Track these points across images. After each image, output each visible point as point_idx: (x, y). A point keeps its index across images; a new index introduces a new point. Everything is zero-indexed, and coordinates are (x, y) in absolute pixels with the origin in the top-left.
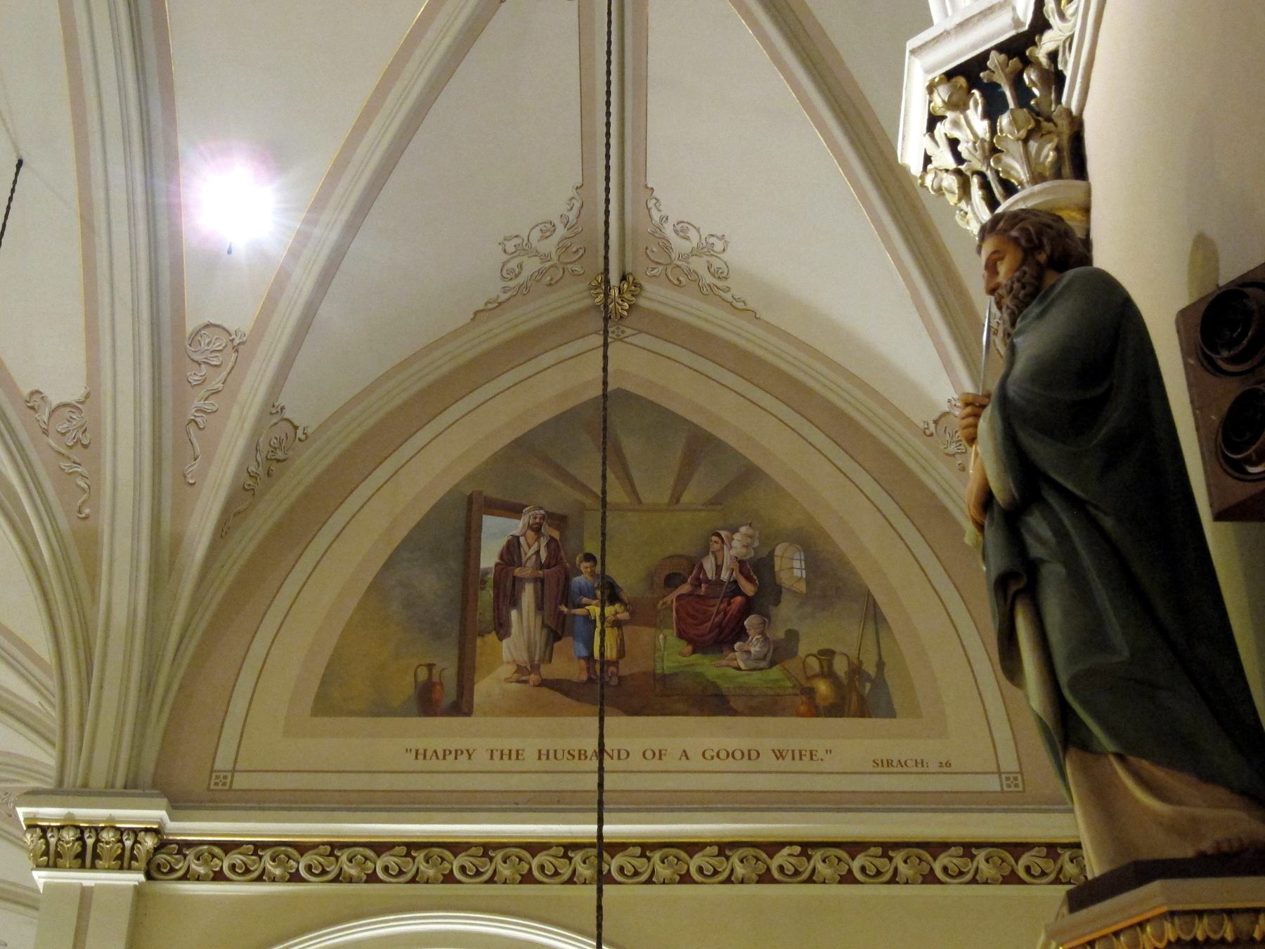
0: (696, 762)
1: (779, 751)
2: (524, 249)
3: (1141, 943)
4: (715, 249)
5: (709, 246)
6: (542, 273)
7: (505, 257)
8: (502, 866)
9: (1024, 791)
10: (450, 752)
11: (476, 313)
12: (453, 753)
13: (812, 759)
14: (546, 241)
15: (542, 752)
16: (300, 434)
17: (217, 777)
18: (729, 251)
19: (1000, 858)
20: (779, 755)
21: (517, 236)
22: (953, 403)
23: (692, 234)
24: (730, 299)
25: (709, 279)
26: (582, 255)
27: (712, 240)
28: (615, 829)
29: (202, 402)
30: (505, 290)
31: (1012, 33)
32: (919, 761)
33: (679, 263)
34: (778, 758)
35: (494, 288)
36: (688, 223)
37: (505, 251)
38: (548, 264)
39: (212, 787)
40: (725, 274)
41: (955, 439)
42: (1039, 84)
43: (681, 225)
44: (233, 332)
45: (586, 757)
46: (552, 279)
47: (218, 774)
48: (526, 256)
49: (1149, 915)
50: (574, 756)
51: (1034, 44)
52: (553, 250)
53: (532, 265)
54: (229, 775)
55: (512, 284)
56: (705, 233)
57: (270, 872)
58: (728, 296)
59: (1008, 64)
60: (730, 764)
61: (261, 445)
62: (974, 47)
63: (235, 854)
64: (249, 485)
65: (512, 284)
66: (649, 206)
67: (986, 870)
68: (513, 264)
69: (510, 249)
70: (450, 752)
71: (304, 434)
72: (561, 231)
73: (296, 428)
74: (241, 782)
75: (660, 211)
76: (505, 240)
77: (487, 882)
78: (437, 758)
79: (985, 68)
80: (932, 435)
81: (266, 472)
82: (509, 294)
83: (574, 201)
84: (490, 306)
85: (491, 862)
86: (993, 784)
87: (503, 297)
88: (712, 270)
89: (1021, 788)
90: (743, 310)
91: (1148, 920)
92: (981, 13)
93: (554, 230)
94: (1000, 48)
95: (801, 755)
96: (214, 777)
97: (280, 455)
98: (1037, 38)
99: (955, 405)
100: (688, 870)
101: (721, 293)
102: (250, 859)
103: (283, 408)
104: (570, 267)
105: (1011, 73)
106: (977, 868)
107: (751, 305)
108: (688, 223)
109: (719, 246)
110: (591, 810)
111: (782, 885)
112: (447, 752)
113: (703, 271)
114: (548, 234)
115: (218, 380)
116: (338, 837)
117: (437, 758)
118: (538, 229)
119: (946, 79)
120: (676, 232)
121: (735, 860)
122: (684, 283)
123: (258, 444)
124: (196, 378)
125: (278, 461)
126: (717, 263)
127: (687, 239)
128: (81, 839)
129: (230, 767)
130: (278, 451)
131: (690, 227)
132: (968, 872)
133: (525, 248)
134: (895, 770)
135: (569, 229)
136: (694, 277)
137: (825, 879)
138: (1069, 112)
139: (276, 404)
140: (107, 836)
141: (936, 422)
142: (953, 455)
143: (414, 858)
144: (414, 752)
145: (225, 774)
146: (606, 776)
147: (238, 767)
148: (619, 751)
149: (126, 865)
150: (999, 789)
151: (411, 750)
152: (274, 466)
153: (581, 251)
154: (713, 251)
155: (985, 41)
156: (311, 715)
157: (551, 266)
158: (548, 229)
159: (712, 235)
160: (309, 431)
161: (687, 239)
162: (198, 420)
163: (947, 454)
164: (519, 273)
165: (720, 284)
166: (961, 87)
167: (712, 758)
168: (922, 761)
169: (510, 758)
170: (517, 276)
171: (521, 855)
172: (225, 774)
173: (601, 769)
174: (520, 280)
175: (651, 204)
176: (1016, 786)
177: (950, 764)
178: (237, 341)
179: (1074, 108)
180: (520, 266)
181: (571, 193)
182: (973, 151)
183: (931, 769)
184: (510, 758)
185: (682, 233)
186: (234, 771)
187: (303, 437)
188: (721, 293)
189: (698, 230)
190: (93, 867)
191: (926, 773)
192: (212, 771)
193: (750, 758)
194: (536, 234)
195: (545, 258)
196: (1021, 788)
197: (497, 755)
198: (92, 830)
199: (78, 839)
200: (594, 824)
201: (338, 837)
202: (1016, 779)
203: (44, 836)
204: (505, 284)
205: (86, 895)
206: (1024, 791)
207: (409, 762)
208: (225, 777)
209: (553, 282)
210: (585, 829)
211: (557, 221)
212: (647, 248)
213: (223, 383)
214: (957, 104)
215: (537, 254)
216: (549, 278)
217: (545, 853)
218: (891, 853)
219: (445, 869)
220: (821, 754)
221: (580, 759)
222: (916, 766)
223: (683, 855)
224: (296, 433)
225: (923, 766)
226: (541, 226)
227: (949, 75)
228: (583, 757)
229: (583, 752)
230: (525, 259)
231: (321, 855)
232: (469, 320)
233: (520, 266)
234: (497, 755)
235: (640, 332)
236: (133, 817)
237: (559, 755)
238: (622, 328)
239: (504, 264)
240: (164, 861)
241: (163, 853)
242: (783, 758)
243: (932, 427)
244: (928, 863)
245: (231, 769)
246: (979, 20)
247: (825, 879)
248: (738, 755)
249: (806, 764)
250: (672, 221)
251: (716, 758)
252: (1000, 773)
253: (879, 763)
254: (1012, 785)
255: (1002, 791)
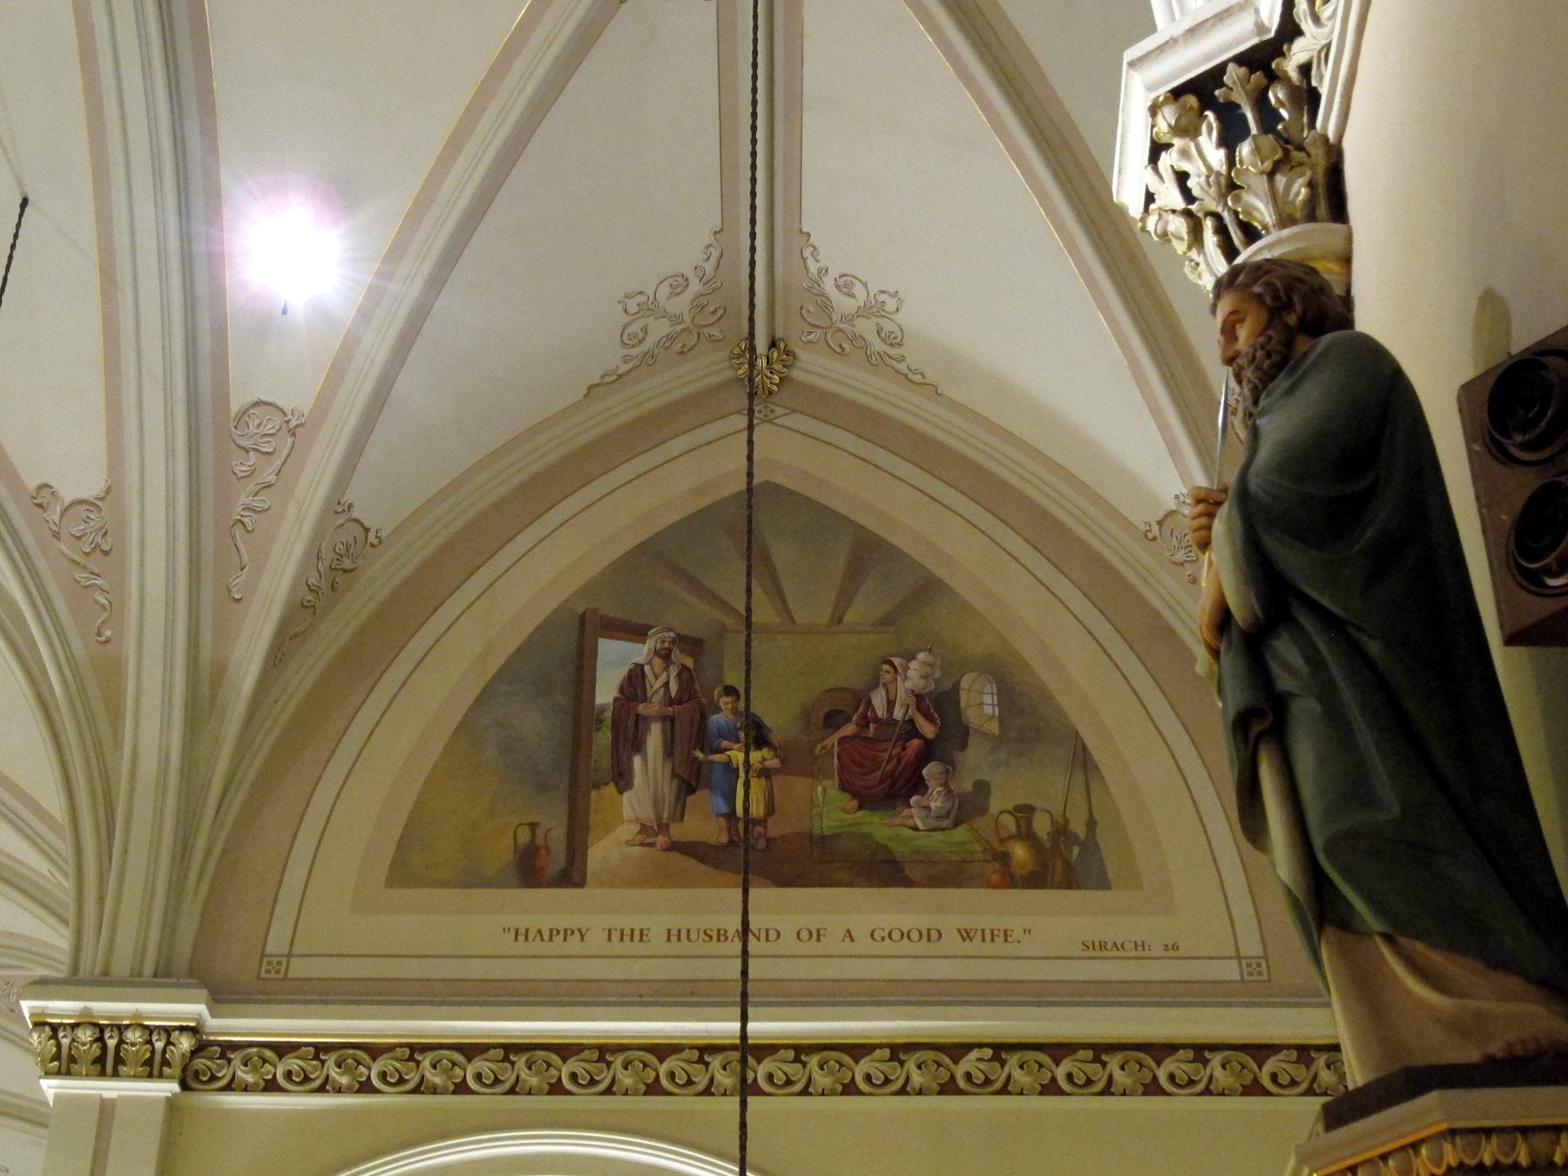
0: (863, 944)
1: (966, 930)
2: (650, 309)
3: (1415, 1169)
4: (886, 308)
5: (879, 305)
6: (672, 338)
7: (626, 319)
8: (622, 1073)
9: (1269, 980)
10: (558, 932)
11: (590, 388)
12: (562, 933)
13: (1006, 940)
14: (676, 299)
15: (672, 932)
16: (372, 538)
17: (269, 963)
18: (903, 311)
19: (1240, 1063)
20: (966, 935)
21: (640, 293)
22: (1182, 499)
23: (858, 290)
24: (905, 371)
25: (878, 346)
26: (722, 316)
27: (882, 297)
28: (762, 1028)
29: (250, 498)
30: (626, 359)
31: (1255, 41)
32: (1139, 943)
33: (842, 326)
34: (964, 940)
35: (612, 357)
36: (853, 276)
37: (626, 311)
38: (679, 328)
39: (263, 975)
40: (898, 340)
41: (1183, 544)
42: (1287, 105)
43: (844, 279)
44: (288, 411)
45: (727, 938)
46: (684, 346)
47: (270, 959)
48: (652, 318)
49: (1424, 1134)
50: (711, 937)
51: (1282, 54)
52: (686, 310)
53: (659, 329)
54: (284, 960)
55: (635, 351)
56: (873, 289)
57: (334, 1081)
58: (902, 367)
59: (1249, 80)
60: (905, 947)
61: (324, 551)
62: (1208, 58)
63: (291, 1058)
64: (309, 601)
65: (635, 351)
66: (805, 255)
67: (1223, 1078)
68: (636, 327)
69: (633, 308)
70: (558, 932)
71: (377, 537)
72: (695, 286)
73: (367, 530)
74: (299, 968)
75: (818, 261)
76: (626, 297)
77: (603, 1093)
78: (542, 939)
79: (1222, 85)
80: (1155, 539)
81: (330, 585)
82: (631, 365)
83: (712, 249)
84: (607, 379)
85: (609, 1068)
86: (1230, 971)
87: (624, 368)
88: (883, 335)
89: (1265, 977)
90: (921, 384)
91: (1423, 1141)
92: (1216, 16)
93: (687, 285)
94: (1240, 59)
95: (992, 936)
96: (265, 963)
97: (347, 564)
98: (1285, 47)
99: (1184, 502)
100: (853, 1078)
101: (894, 363)
102: (309, 1065)
103: (350, 506)
104: (706, 330)
105: (1254, 90)
106: (1211, 1076)
107: (931, 378)
108: (853, 276)
109: (891, 305)
110: (732, 1004)
111: (969, 1097)
112: (555, 932)
113: (871, 336)
114: (679, 290)
115: (270, 471)
116: (419, 1037)
117: (542, 939)
118: (666, 283)
119: (1172, 98)
120: (838, 287)
121: (911, 1066)
122: (848, 350)
123: (319, 550)
124: (243, 468)
125: (345, 571)
126: (888, 326)
127: (852, 296)
128: (100, 1040)
129: (285, 950)
130: (344, 559)
131: (855, 281)
132: (1200, 1081)
133: (651, 307)
134: (1110, 954)
135: (705, 284)
136: (860, 343)
137: (1022, 1089)
138: (1325, 139)
139: (342, 501)
140: (133, 1036)
141: (1160, 523)
142: (1182, 564)
143: (513, 1064)
144: (513, 932)
145: (279, 959)
146: (751, 962)
147: (295, 951)
148: (767, 931)
149: (156, 1072)
150: (1238, 978)
151: (509, 929)
152: (340, 577)
153: (721, 312)
154: (884, 311)
155: (1221, 51)
156: (386, 886)
157: (683, 330)
158: (679, 284)
159: (883, 292)
160: (383, 534)
161: (852, 296)
162: (245, 520)
163: (1174, 563)
164: (644, 339)
165: (892, 351)
166: (1191, 108)
167: (883, 939)
168: (1143, 943)
169: (632, 940)
170: (640, 342)
171: (645, 1059)
172: (279, 959)
173: (745, 953)
174: (645, 347)
175: (807, 252)
176: (1260, 973)
177: (1178, 947)
178: (293, 423)
179: (1331, 134)
180: (645, 330)
181: (708, 239)
182: (1206, 188)
183: (1154, 953)
184: (632, 940)
185: (845, 289)
186: (290, 955)
187: (375, 542)
188: (894, 363)
189: (865, 285)
190: (116, 1075)
191: (1148, 958)
192: (263, 955)
193: (929, 940)
194: (664, 290)
195: (676, 319)
196: (1265, 977)
197: (616, 936)
198: (114, 1029)
199: (96, 1040)
200: (736, 1021)
201: (419, 1037)
202: (1259, 965)
203: (54, 1036)
204: (627, 352)
205: (106, 1109)
206: (1269, 980)
207: (507, 944)
208: (279, 963)
209: (685, 350)
210: (725, 1028)
211: (690, 274)
212: (802, 308)
213: (277, 475)
214: (1186, 129)
215: (665, 315)
216: (680, 345)
217: (675, 1056)
218: (1104, 1058)
219: (551, 1077)
220: (1017, 934)
221: (719, 940)
222: (1136, 949)
223: (846, 1059)
224: (367, 537)
225: (1144, 949)
226: (671, 280)
227: (1177, 93)
228: (722, 938)
229: (722, 932)
230: (650, 321)
231: (397, 1060)
232: (581, 397)
233: (645, 330)
234: (616, 936)
235: (794, 411)
236: (165, 1013)
237: (693, 936)
238: (771, 407)
239: (625, 327)
240: (203, 1067)
241: (202, 1057)
242: (971, 940)
243: (1155, 529)
244: (1151, 1070)
245: (286, 953)
246: (1214, 25)
247: (1022, 1089)
248: (915, 935)
249: (999, 947)
250: (833, 273)
251: (887, 939)
252: (1239, 958)
253: (1090, 945)
254: (1255, 973)
255: (1243, 981)
